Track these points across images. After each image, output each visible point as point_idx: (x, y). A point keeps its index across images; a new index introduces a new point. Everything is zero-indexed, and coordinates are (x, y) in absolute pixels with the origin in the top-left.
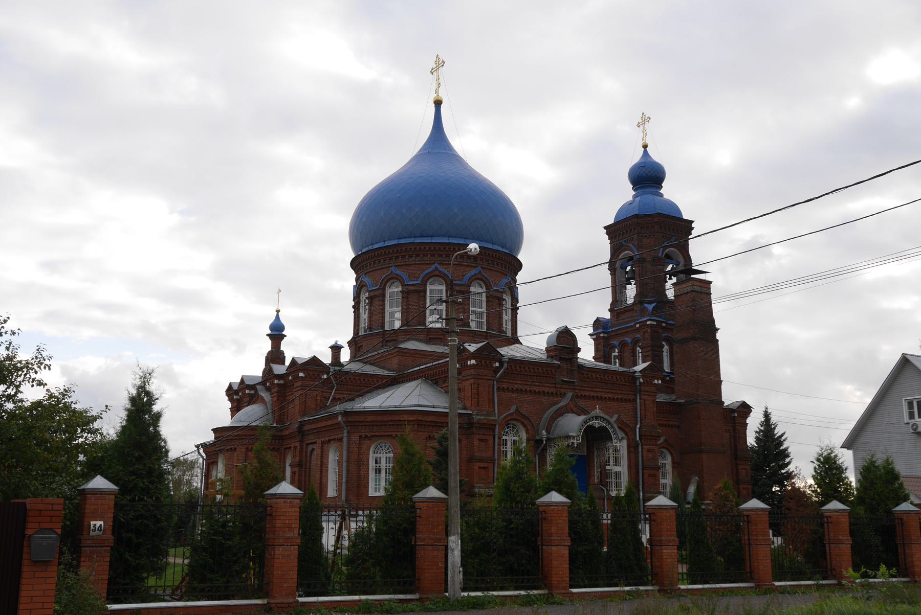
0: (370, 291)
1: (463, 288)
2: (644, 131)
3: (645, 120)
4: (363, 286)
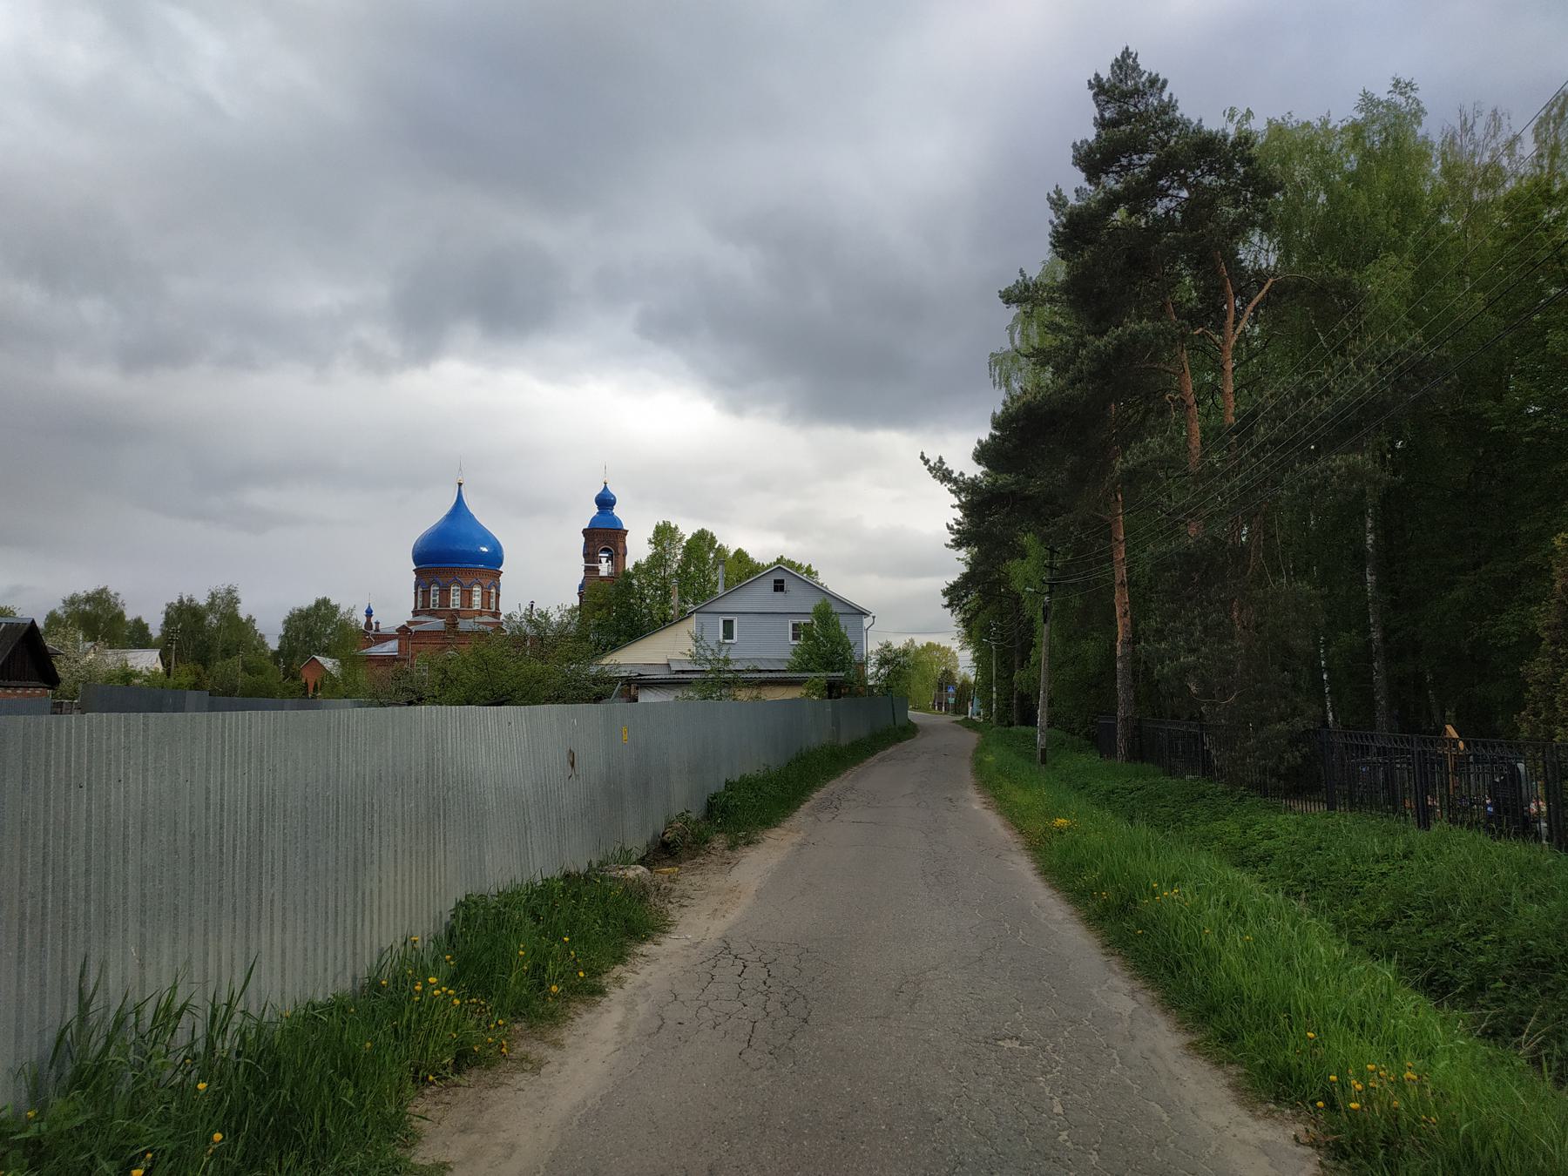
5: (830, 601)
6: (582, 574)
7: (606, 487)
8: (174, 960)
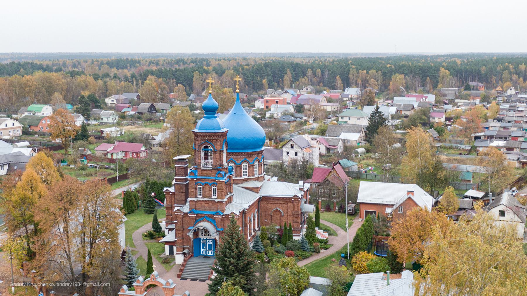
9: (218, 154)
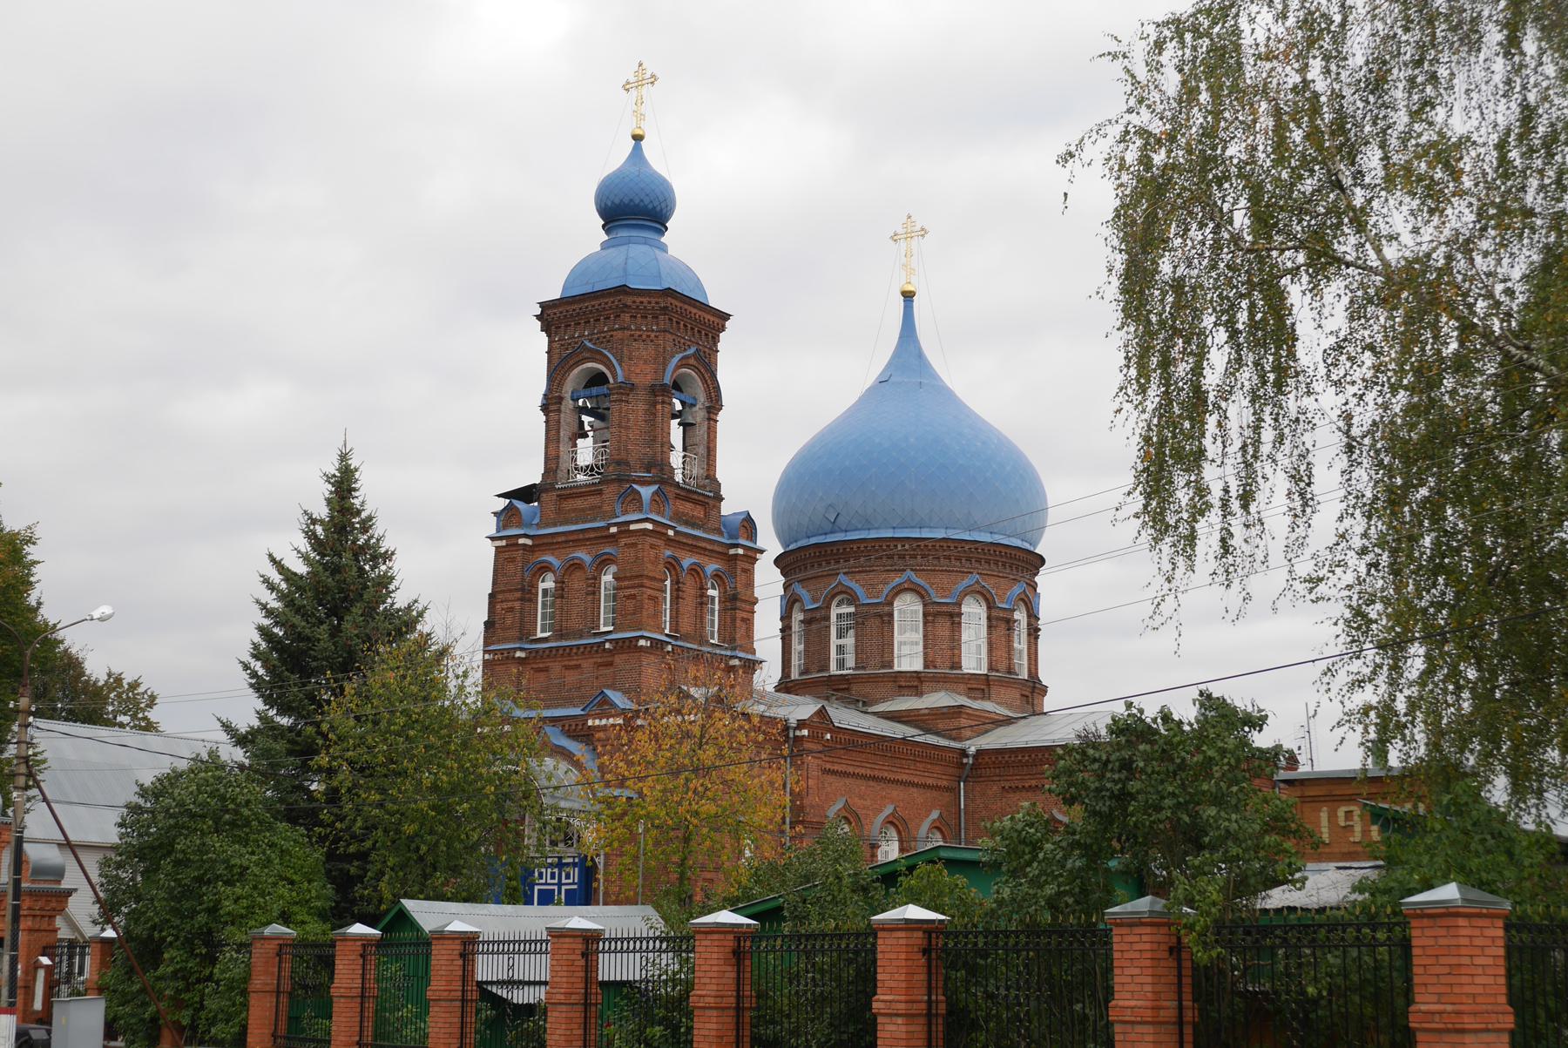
0: (805, 611)
1: (950, 609)
2: (640, 102)
3: (643, 80)
4: (796, 601)
5: (1203, 687)
6: (542, 340)
7: (637, 153)
8: (1302, 495)
9: (641, 407)
